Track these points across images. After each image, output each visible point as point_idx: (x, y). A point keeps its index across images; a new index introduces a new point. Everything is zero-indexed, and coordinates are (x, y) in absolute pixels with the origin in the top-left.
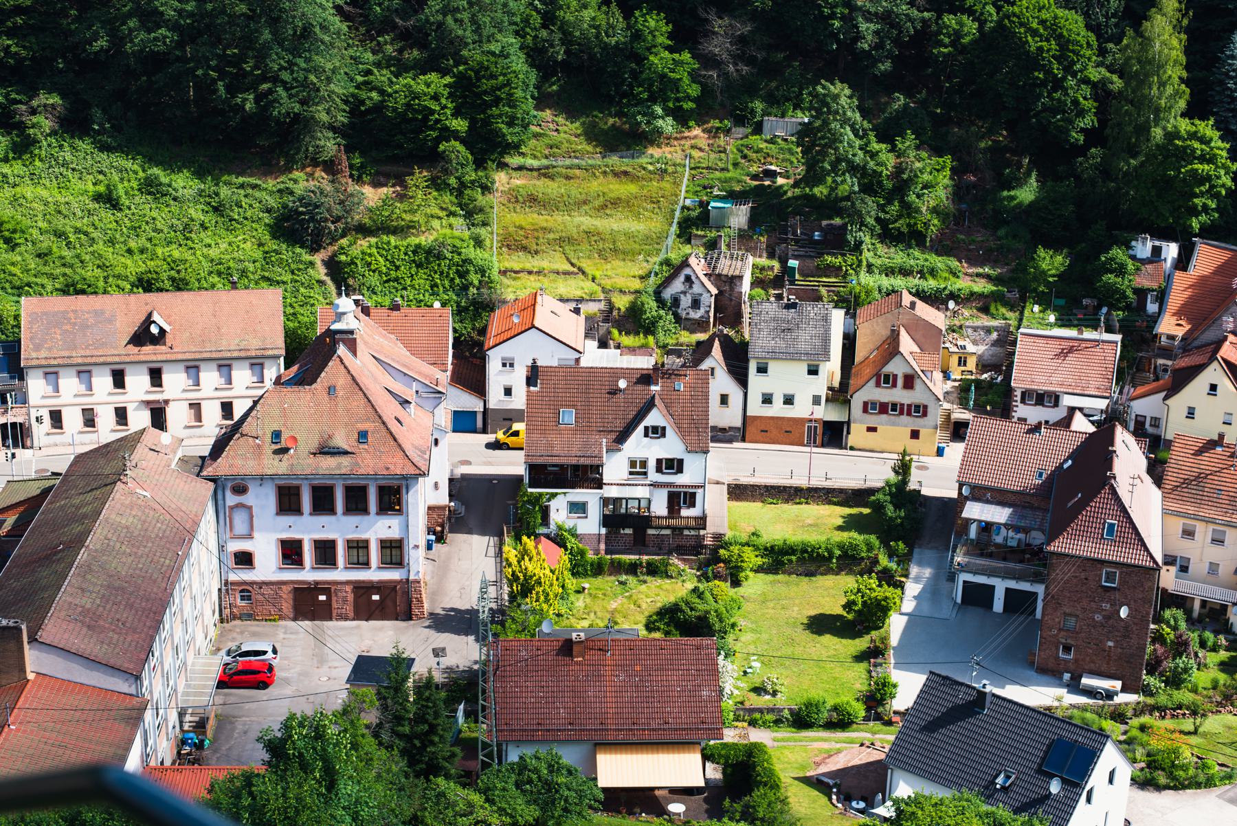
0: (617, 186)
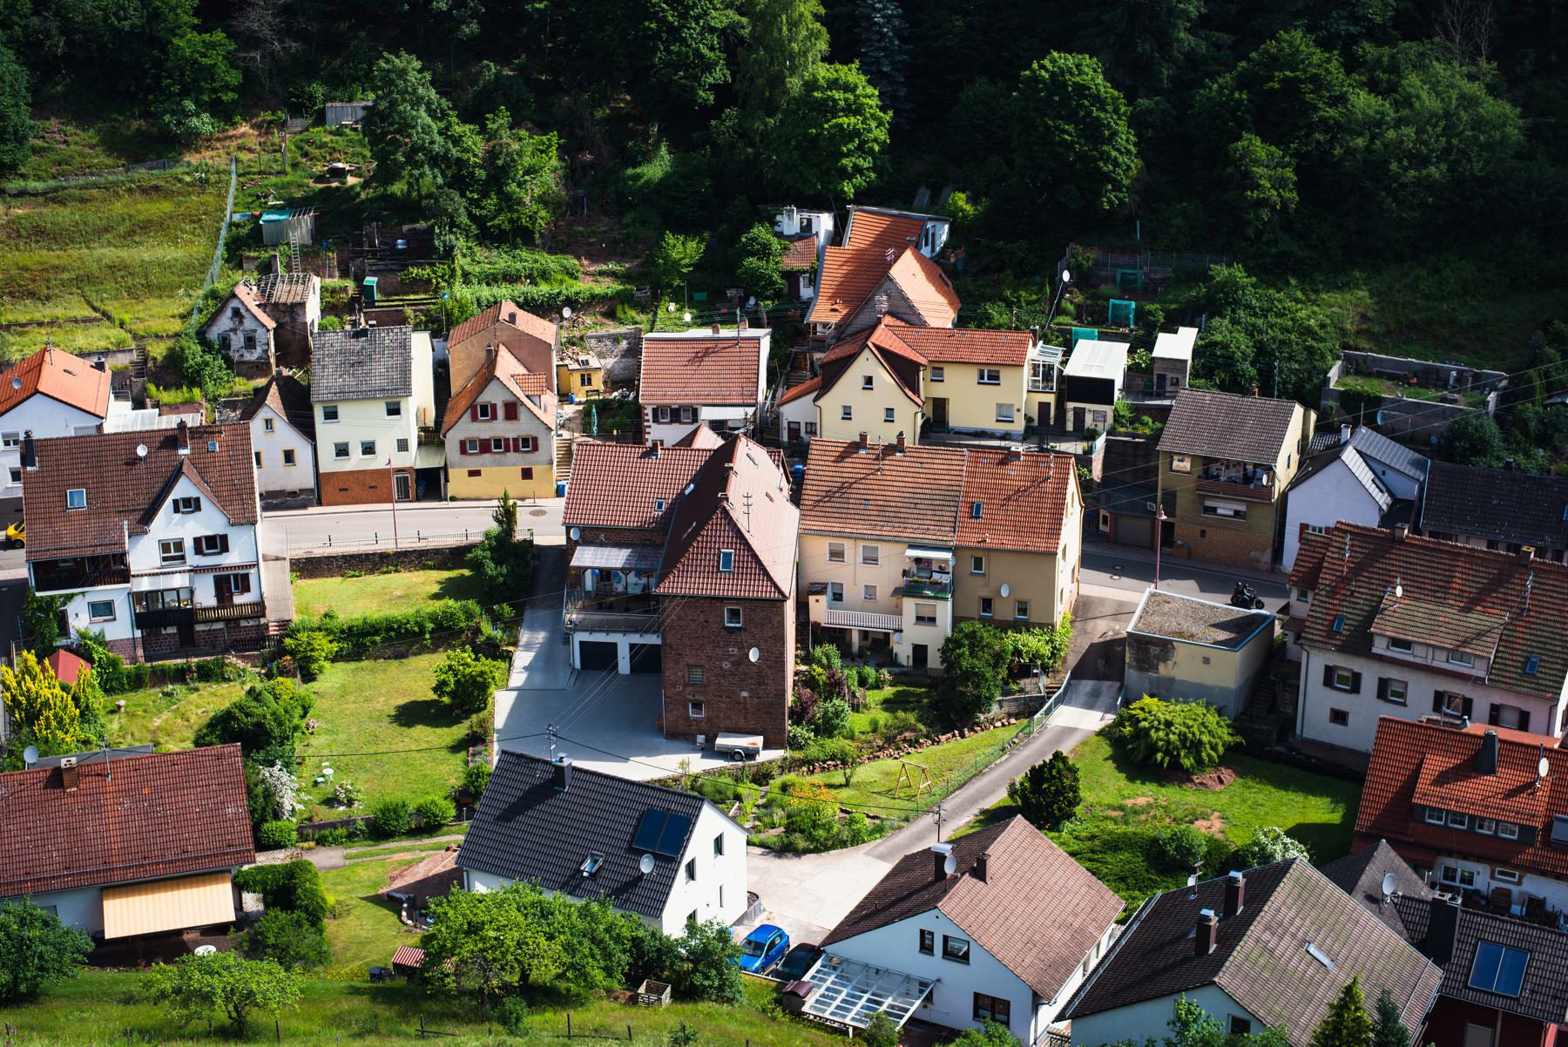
0: (147, 206)
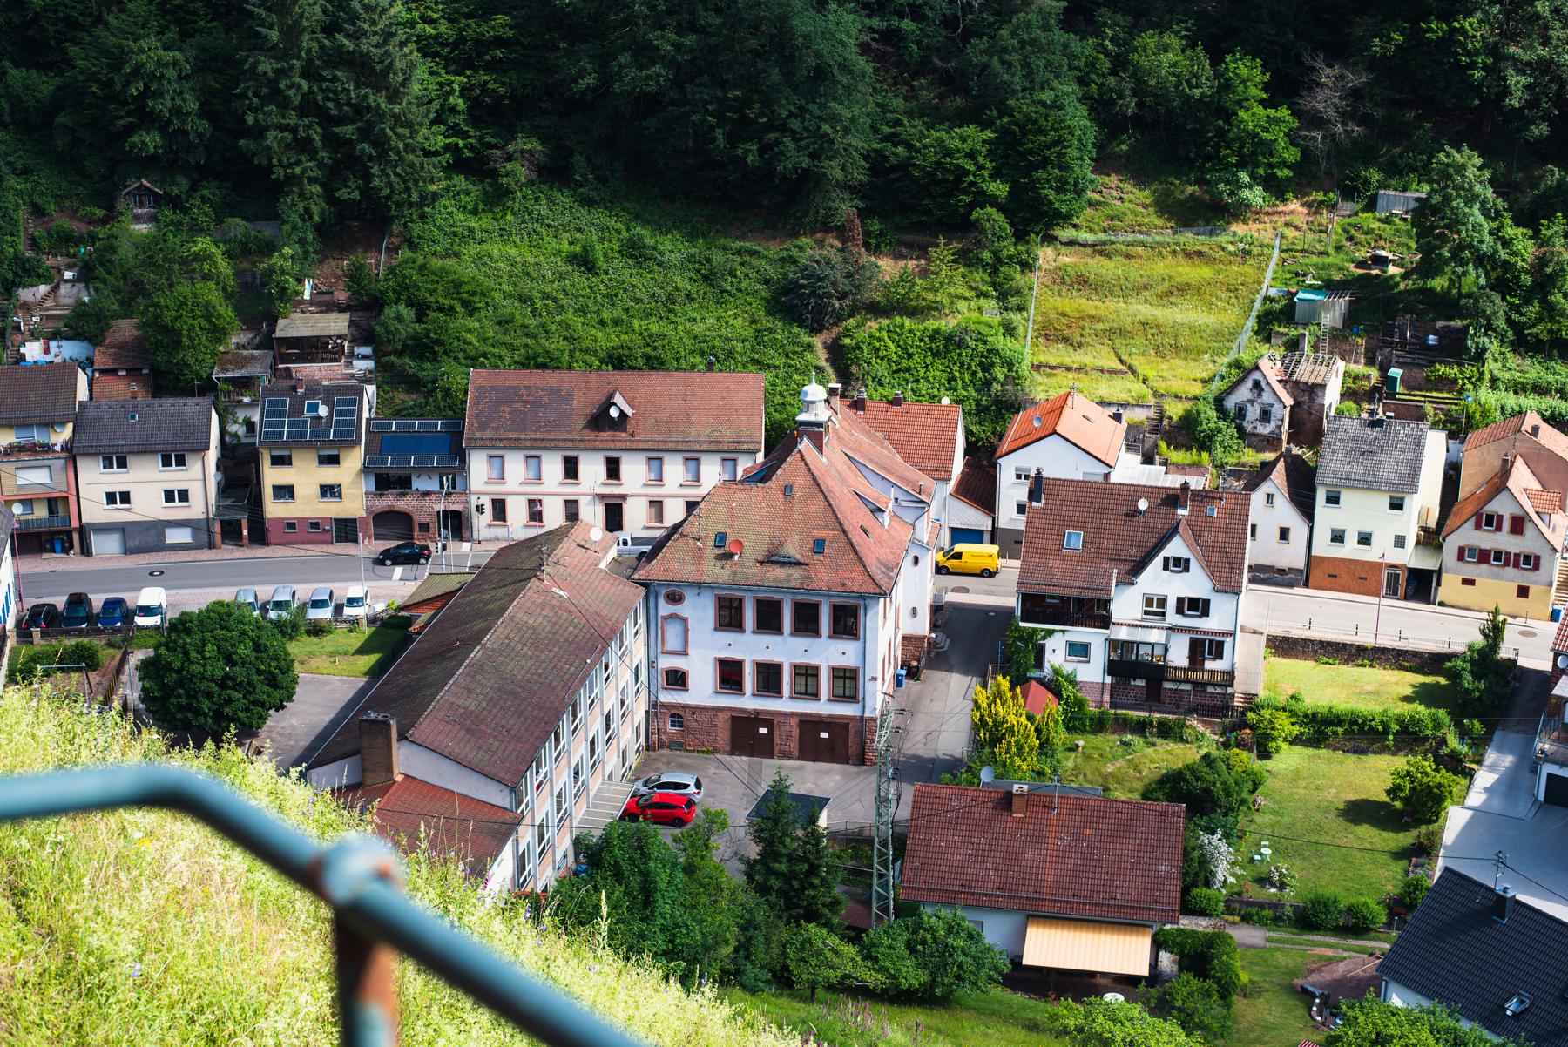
0: (1187, 269)
